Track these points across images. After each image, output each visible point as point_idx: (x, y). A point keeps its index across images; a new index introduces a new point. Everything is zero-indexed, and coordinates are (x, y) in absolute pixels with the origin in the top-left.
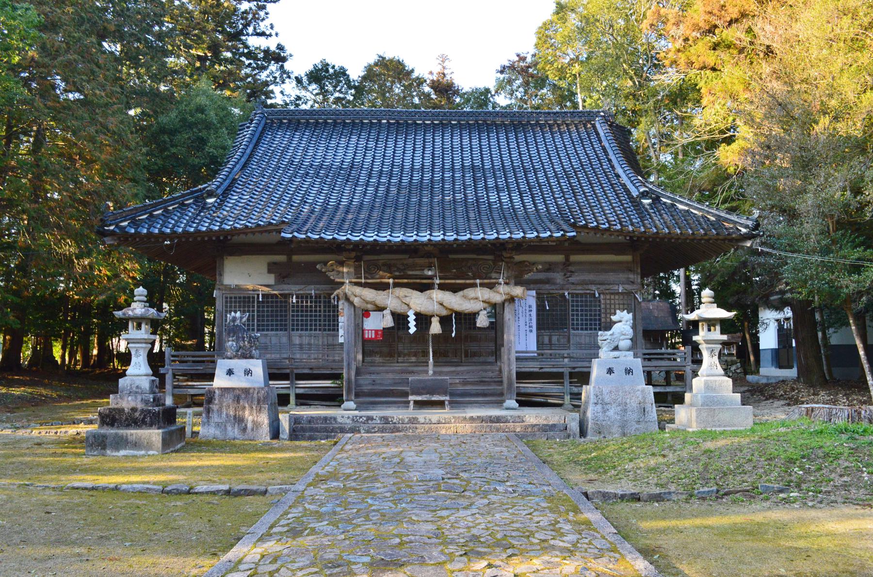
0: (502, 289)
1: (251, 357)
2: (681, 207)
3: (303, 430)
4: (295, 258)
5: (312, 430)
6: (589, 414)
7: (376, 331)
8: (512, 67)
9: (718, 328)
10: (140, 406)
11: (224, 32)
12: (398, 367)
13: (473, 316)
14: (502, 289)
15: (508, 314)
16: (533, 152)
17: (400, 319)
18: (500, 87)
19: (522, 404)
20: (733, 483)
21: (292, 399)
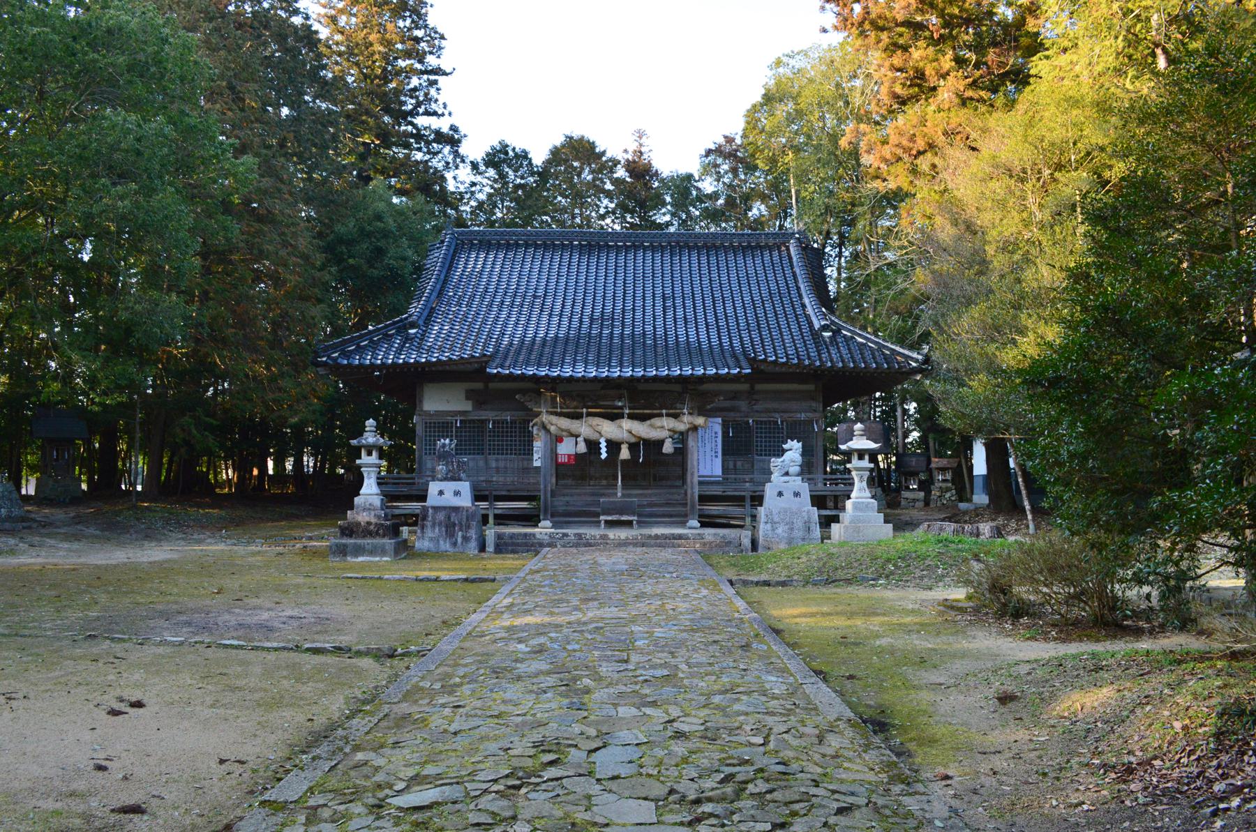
0: (686, 418)
1: (460, 480)
2: (860, 340)
3: (506, 544)
5: (513, 544)
6: (761, 533)
7: (569, 456)
8: (718, 151)
9: (867, 457)
10: (373, 520)
11: (386, 99)
12: (588, 490)
13: (660, 443)
15: (691, 443)
16: (724, 279)
17: (593, 445)
18: (706, 170)
19: (704, 525)
20: (840, 574)
21: (491, 520)
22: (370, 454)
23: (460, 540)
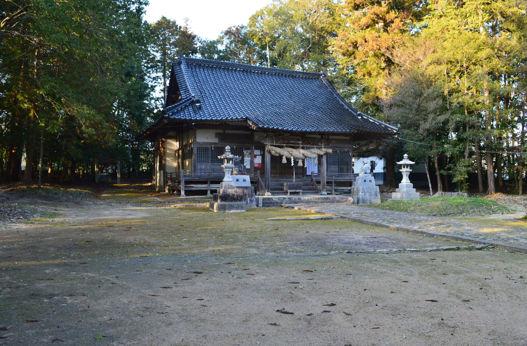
4: (227, 131)
7: (259, 164)
14: (324, 150)
20: (449, 211)
22: (407, 167)
23: (249, 202)
